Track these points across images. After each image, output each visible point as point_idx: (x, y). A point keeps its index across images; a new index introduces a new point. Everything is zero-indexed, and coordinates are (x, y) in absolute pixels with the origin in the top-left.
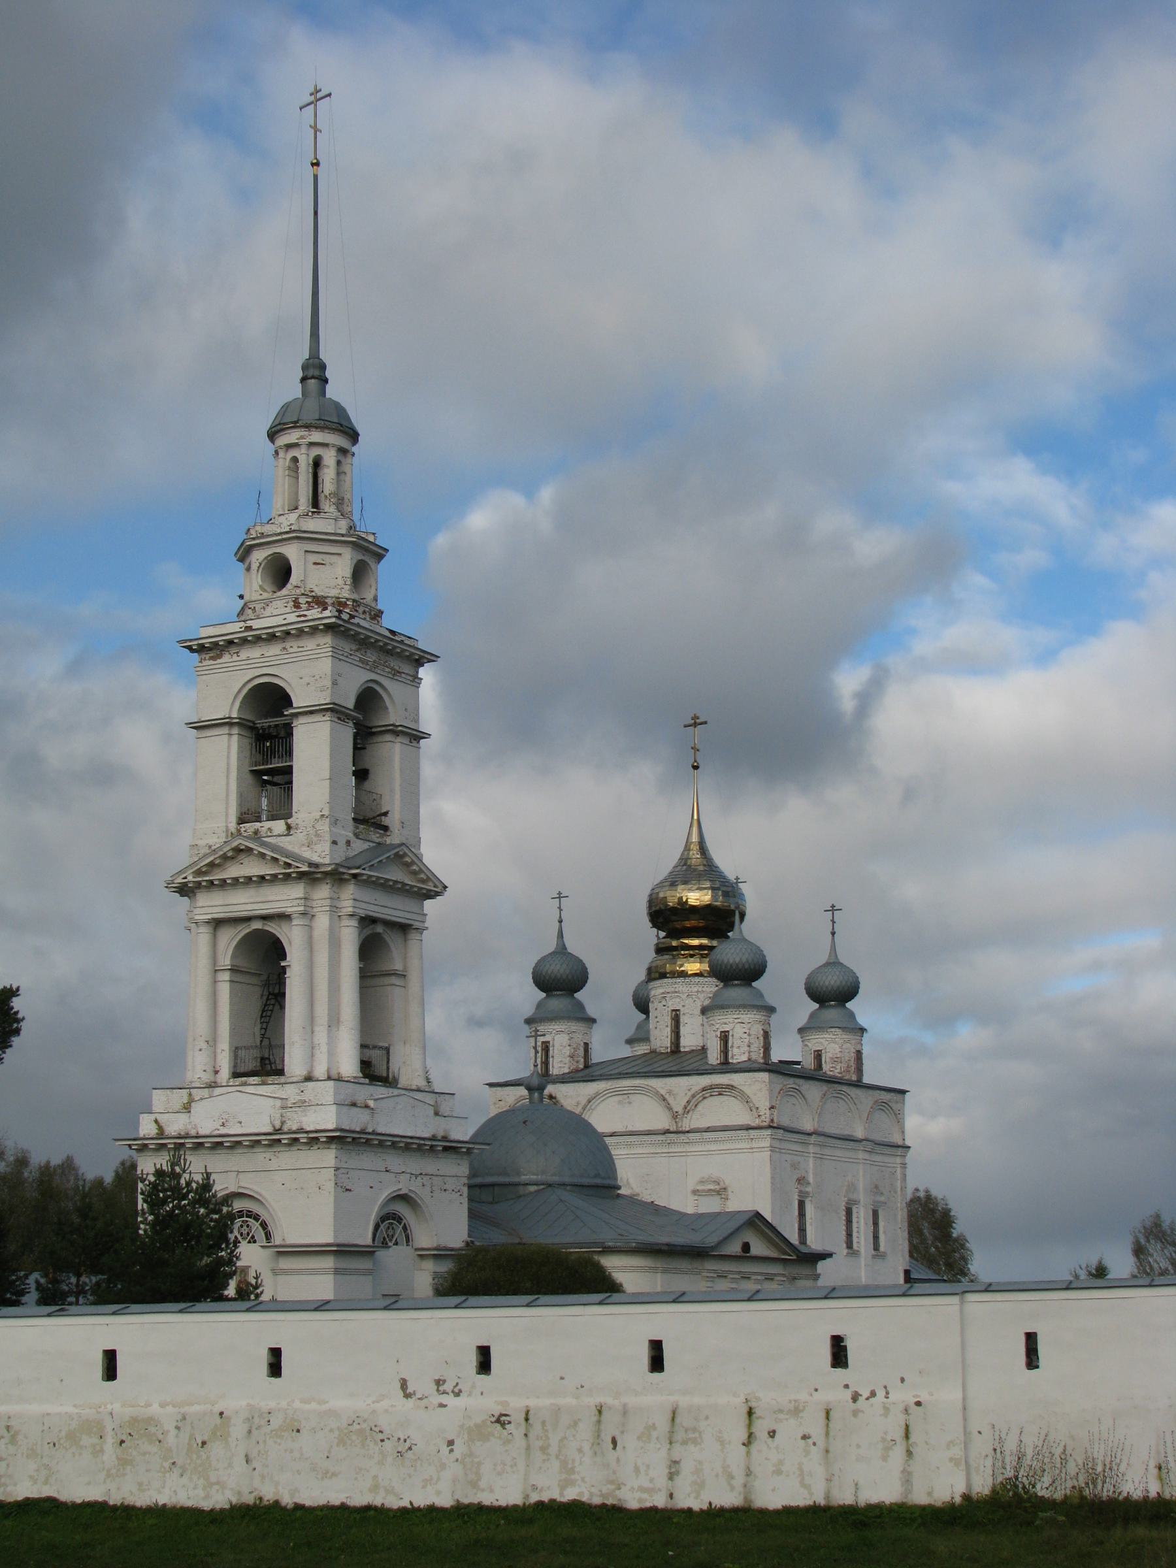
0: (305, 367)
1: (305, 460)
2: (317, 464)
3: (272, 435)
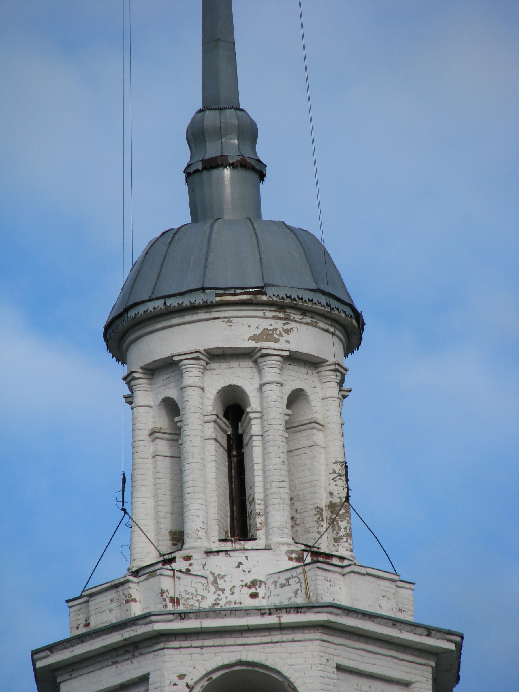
0: (196, 136)
1: (201, 394)
2: (233, 409)
3: (120, 333)
